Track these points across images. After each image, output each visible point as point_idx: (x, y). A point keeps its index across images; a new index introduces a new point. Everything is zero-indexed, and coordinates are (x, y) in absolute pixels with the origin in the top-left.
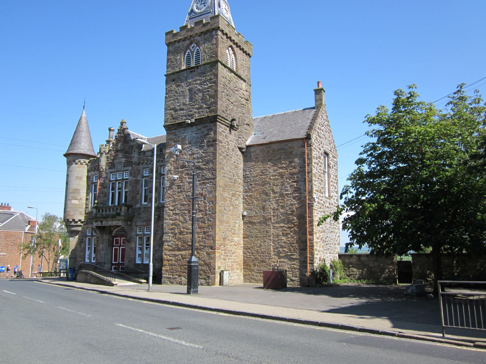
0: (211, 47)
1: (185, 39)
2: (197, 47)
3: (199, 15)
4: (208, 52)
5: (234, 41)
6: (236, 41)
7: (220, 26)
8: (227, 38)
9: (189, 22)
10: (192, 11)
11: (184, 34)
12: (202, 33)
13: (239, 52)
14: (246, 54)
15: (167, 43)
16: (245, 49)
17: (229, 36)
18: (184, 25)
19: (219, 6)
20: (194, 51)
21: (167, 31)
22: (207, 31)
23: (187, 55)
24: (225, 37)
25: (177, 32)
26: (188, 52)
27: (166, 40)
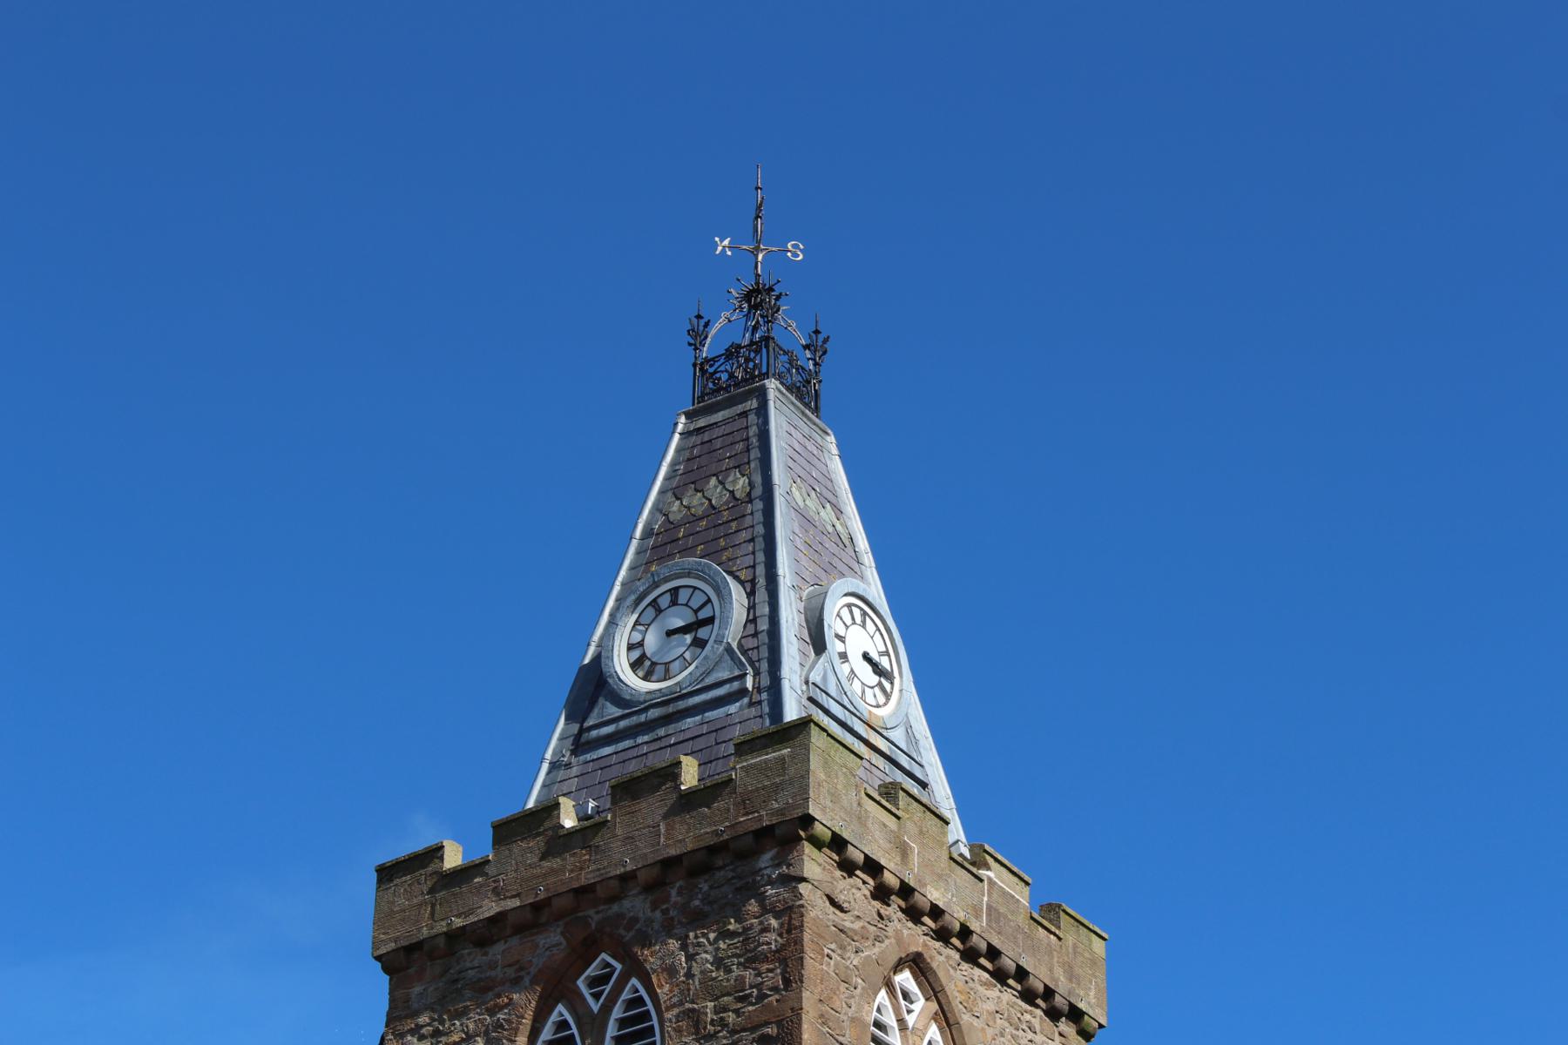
0: (740, 979)
1: (536, 916)
2: (634, 981)
3: (654, 713)
4: (723, 1023)
5: (936, 912)
6: (957, 914)
7: (813, 810)
8: (881, 894)
9: (575, 771)
10: (594, 684)
11: (534, 873)
12: (669, 863)
13: (990, 1006)
14: (1053, 1014)
15: (383, 951)
16: (1040, 975)
17: (890, 879)
18: (531, 804)
19: (817, 640)
20: (607, 1009)
21: (388, 855)
22: (712, 850)
23: (623, 1023)
24: (855, 891)
25: (476, 857)
26: (554, 1017)
27: (383, 918)
